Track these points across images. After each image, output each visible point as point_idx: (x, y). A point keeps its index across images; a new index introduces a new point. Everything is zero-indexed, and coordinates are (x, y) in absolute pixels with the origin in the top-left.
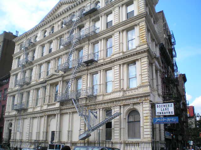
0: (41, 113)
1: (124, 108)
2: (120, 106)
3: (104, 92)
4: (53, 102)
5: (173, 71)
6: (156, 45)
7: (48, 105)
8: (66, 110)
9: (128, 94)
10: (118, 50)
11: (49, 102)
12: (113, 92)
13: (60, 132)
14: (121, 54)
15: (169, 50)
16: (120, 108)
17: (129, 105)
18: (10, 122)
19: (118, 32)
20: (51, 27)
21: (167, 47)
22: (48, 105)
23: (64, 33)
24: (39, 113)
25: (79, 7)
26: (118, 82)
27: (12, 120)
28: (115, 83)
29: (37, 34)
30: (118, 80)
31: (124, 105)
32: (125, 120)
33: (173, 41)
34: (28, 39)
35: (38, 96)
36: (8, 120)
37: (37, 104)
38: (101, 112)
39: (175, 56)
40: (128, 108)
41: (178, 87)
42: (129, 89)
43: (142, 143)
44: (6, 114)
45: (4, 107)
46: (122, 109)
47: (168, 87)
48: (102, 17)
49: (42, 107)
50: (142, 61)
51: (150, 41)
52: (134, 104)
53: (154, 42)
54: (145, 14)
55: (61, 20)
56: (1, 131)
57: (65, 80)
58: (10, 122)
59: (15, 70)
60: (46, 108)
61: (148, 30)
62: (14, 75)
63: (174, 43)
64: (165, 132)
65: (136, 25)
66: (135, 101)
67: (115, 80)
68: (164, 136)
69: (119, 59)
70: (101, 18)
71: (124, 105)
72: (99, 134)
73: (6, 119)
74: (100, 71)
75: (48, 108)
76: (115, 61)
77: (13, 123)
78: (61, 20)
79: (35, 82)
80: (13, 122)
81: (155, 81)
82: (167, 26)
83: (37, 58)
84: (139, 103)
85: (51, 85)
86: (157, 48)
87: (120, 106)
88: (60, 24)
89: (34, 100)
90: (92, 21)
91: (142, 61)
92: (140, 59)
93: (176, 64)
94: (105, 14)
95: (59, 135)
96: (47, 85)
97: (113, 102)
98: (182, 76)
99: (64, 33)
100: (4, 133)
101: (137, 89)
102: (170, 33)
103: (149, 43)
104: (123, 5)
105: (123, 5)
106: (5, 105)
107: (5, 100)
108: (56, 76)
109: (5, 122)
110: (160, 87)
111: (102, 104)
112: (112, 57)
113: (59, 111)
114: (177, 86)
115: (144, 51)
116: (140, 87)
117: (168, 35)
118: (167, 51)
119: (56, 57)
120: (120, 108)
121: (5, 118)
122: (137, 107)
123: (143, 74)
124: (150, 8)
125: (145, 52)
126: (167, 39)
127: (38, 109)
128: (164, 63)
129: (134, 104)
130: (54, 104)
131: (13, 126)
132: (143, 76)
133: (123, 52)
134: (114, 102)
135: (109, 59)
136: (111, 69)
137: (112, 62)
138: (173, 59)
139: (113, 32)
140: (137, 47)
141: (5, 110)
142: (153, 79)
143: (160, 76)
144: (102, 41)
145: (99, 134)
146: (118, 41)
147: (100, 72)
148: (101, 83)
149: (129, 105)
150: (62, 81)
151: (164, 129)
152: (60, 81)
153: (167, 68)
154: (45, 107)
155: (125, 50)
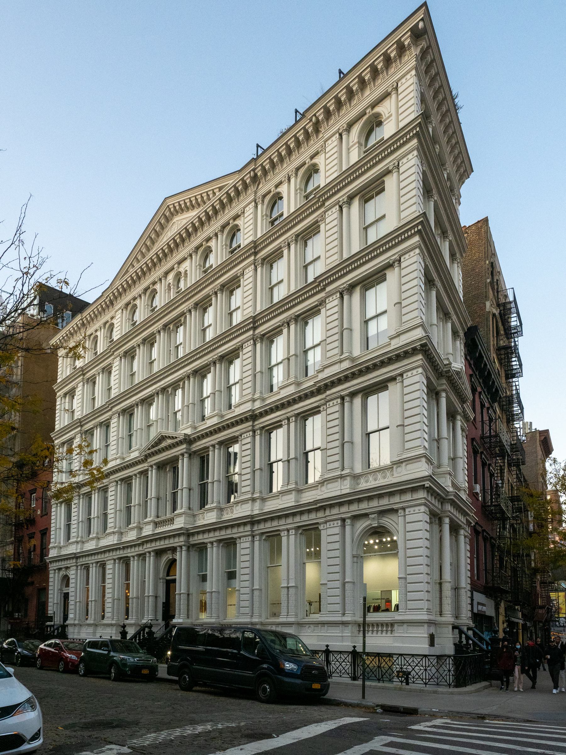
0: (139, 545)
1: (352, 525)
2: (343, 520)
3: (301, 481)
4: (169, 516)
5: (510, 418)
6: (455, 333)
7: (156, 524)
8: (200, 537)
9: (364, 485)
10: (336, 351)
11: (158, 517)
12: (323, 482)
13: (188, 595)
14: (346, 365)
15: (499, 349)
16: (343, 526)
17: (366, 515)
18: (62, 573)
19: (338, 295)
20: (226, 231)
21: (493, 342)
22: (156, 524)
23: (183, 308)
24: (135, 546)
25: (222, 219)
26: (337, 450)
27: (67, 568)
28: (330, 452)
29: (112, 318)
30: (337, 443)
31: (356, 518)
32: (355, 559)
33: (514, 322)
34: (264, 196)
35: (129, 499)
36: (60, 569)
37: (129, 522)
38: (292, 538)
39: (519, 373)
40: (364, 525)
41: (522, 467)
42: (368, 471)
43: (402, 623)
44: (53, 553)
45: (46, 533)
46: (348, 528)
47: (490, 465)
48: (289, 245)
49: (140, 529)
50: (408, 519)
51: (435, 321)
52: (382, 513)
53: (449, 325)
54: (415, 128)
55: (172, 269)
56: (44, 600)
57: (195, 452)
58: (62, 573)
59: (66, 429)
60: (151, 533)
61: (429, 282)
62: (63, 443)
63: (519, 331)
64: (472, 594)
65: (390, 266)
66: (385, 502)
67: (330, 445)
68: (469, 607)
69: (340, 381)
70: (285, 252)
71: (356, 518)
72: (288, 601)
73: (52, 567)
74: (288, 419)
75: (156, 532)
76: (328, 386)
77: (71, 577)
78: (172, 269)
79: (118, 462)
80: (72, 573)
81: (445, 445)
82: (500, 273)
83: (117, 390)
84: (394, 511)
85: (161, 466)
86: (458, 343)
87: (343, 520)
88: (171, 281)
89: (120, 511)
90: (262, 264)
91: (406, 382)
92: (401, 375)
93: (518, 394)
94: (297, 236)
95: (188, 605)
96: (150, 469)
97: (323, 508)
98: (538, 435)
99: (183, 308)
100: (50, 604)
101: (390, 468)
102: (506, 296)
103: (431, 325)
104: (351, 198)
105: (351, 198)
106: (47, 528)
107: (46, 513)
108: (169, 441)
109: (51, 576)
110: (462, 464)
111: (294, 514)
112: (321, 376)
113: (182, 539)
114: (518, 464)
115: (414, 349)
116: (398, 463)
117: (498, 305)
118: (493, 355)
119: (169, 386)
120: (343, 526)
121: (51, 562)
122: (387, 521)
123: (407, 422)
124: (439, 202)
125: (414, 351)
126: (494, 315)
127: (132, 536)
128: (480, 393)
129: (382, 513)
130: (171, 521)
131: (71, 585)
132: (407, 430)
133: (353, 360)
134: (325, 510)
135: (312, 383)
136: (319, 412)
137: (320, 390)
138: (510, 385)
139: (323, 295)
140: (391, 339)
141: (50, 543)
142: (438, 440)
143: (463, 430)
144: (292, 327)
145: (288, 601)
146: (336, 323)
147: (289, 424)
148: (292, 455)
149: (366, 515)
150: (186, 455)
151: (469, 587)
152: (182, 455)
153: (488, 409)
154: (148, 531)
155: (357, 352)
